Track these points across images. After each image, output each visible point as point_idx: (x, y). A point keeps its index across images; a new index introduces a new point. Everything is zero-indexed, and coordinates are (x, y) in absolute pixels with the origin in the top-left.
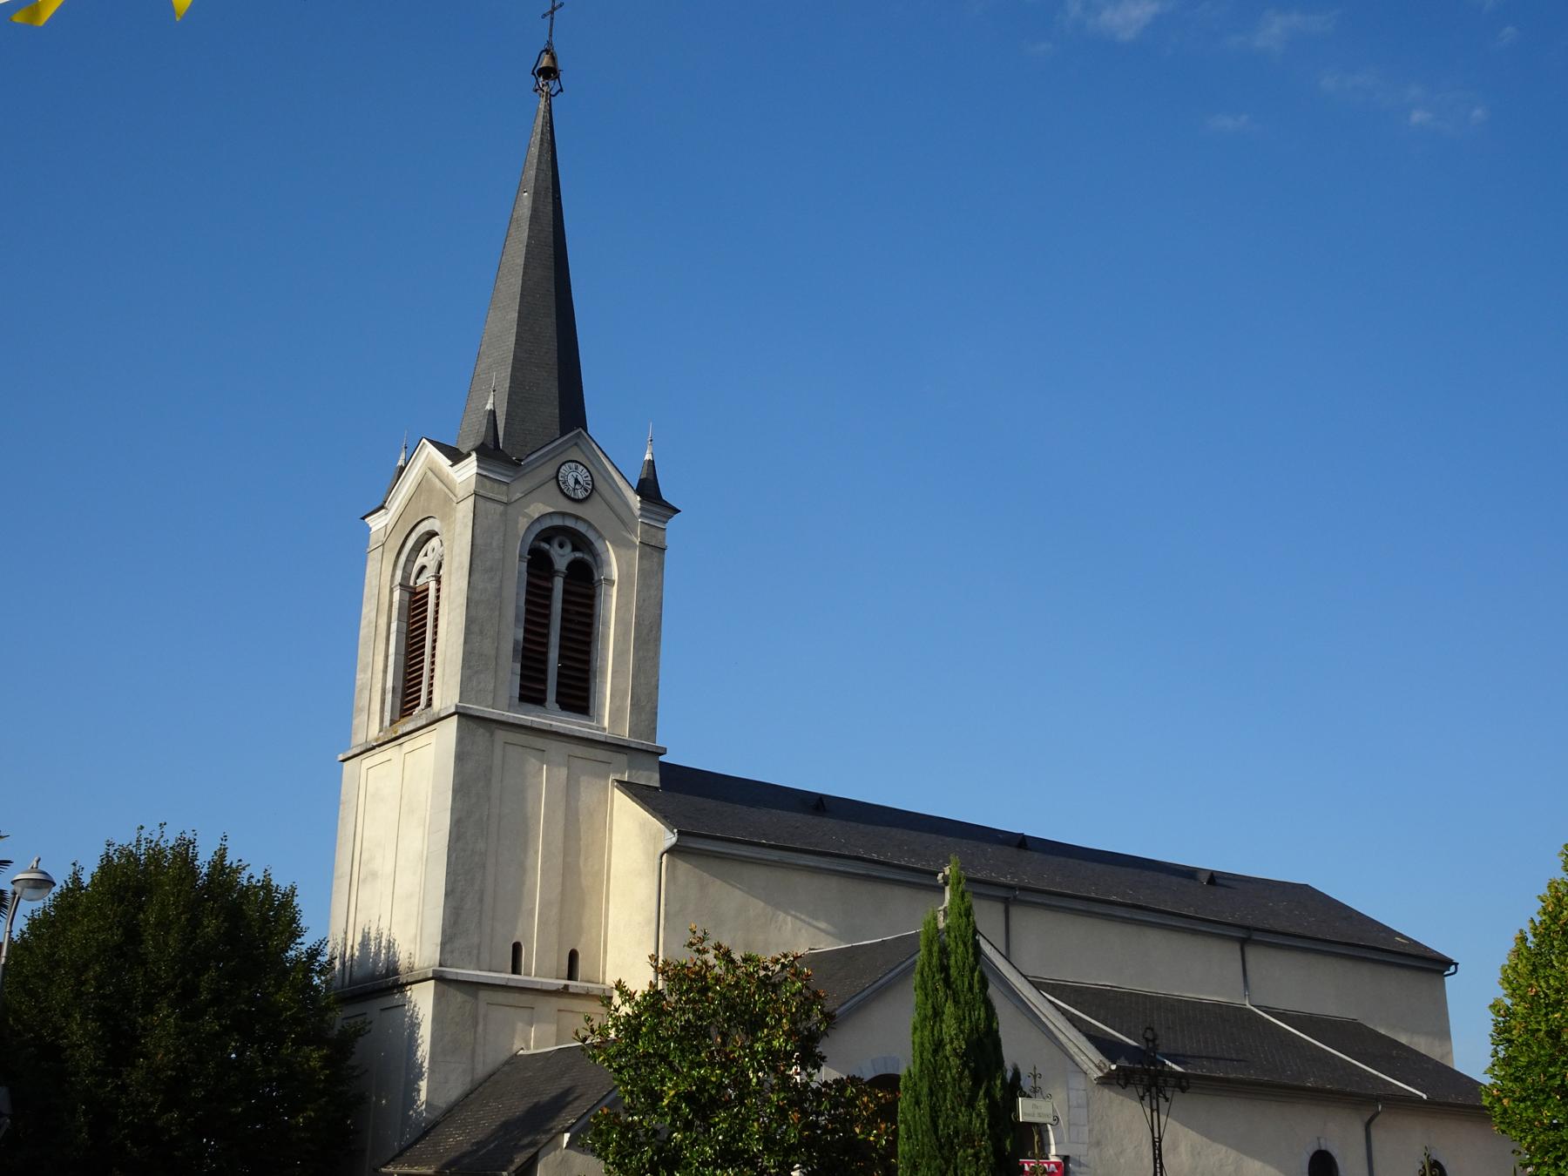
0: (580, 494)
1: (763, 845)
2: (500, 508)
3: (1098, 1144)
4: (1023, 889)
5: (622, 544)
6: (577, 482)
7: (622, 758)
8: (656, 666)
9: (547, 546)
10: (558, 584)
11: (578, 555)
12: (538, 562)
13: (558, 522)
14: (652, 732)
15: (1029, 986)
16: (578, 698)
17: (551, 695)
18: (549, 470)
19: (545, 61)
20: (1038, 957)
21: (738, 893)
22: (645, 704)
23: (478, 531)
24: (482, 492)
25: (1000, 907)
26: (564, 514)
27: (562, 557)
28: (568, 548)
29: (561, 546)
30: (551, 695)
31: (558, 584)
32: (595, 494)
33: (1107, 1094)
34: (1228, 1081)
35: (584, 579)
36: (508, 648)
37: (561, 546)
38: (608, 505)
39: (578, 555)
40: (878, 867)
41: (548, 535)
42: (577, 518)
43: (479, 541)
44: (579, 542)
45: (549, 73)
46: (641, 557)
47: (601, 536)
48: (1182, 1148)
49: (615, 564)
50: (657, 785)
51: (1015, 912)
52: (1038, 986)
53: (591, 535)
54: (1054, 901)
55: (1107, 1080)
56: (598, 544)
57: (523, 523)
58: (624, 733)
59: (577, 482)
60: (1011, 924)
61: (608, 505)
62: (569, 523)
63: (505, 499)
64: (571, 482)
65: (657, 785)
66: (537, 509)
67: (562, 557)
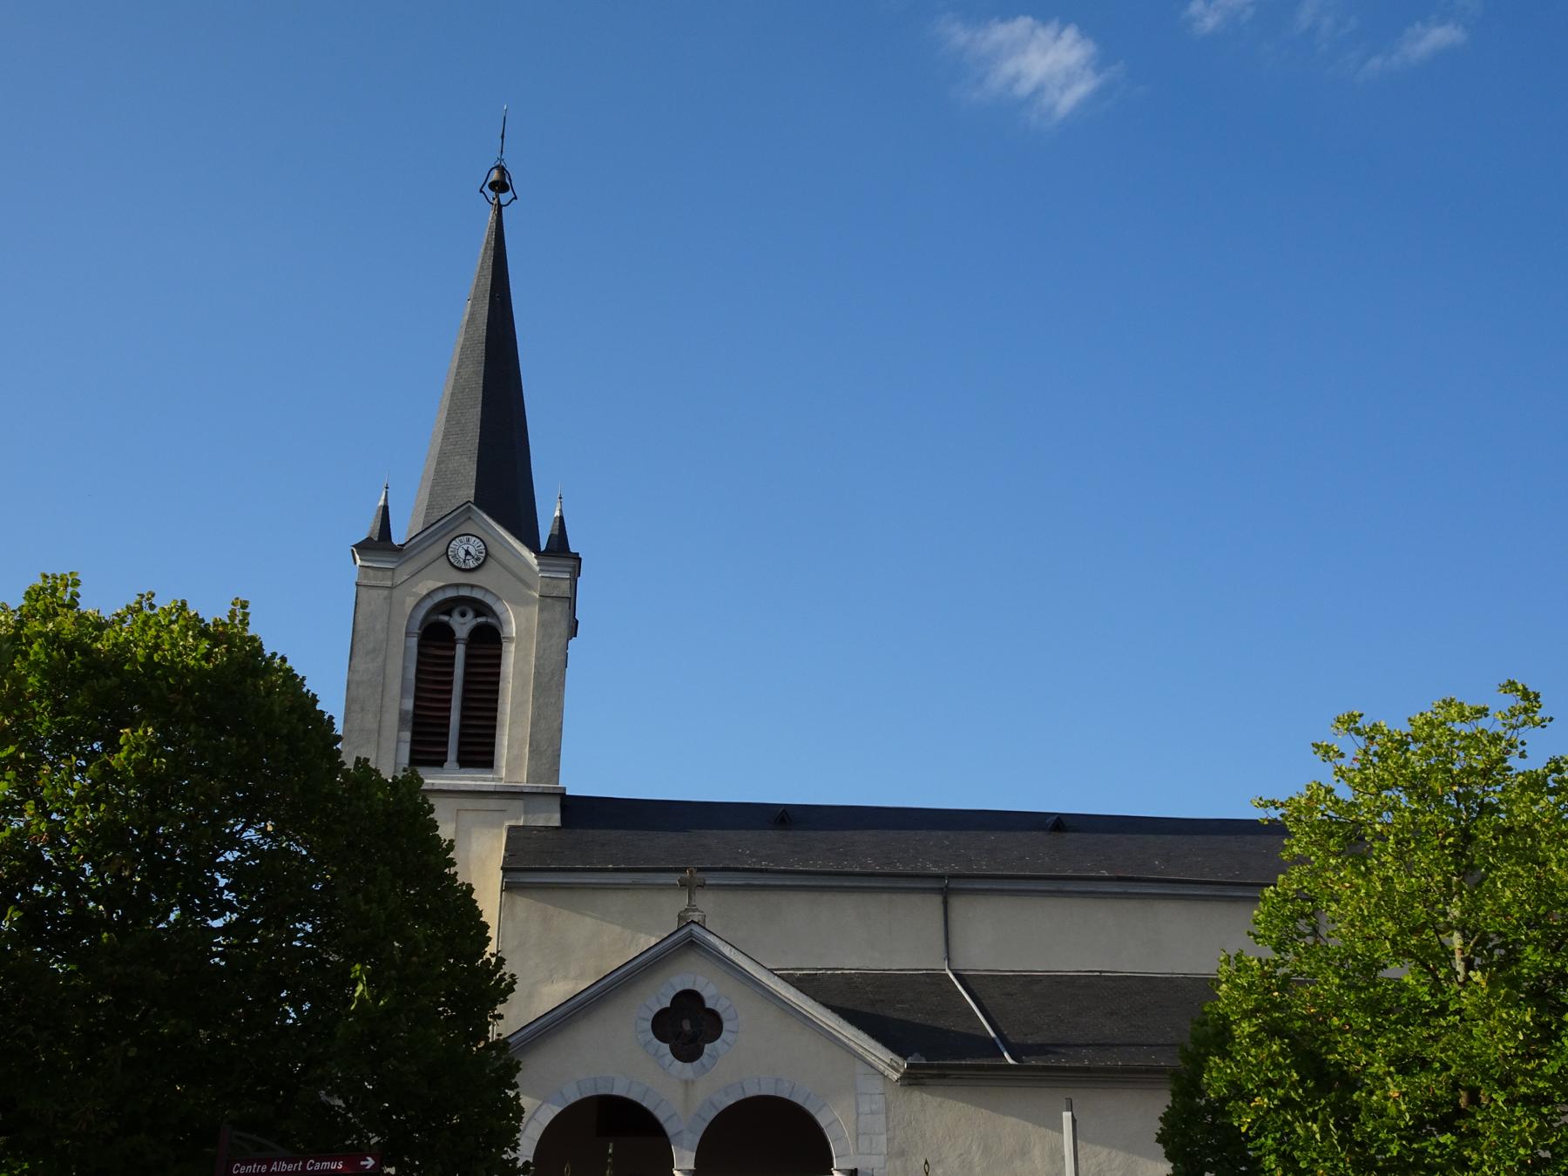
0: (472, 564)
1: (607, 870)
2: (386, 592)
3: (902, 1153)
4: (953, 877)
5: (520, 601)
6: (467, 553)
7: (518, 804)
8: (560, 711)
9: (445, 618)
10: (460, 650)
11: (481, 620)
12: (433, 636)
13: (451, 593)
14: (555, 772)
15: (780, 981)
16: (479, 753)
17: (452, 754)
18: (439, 548)
19: (495, 176)
20: (771, 944)
21: (588, 920)
22: (546, 748)
23: (360, 618)
24: (365, 582)
25: (937, 900)
26: (457, 586)
27: (463, 626)
28: (470, 615)
29: (463, 615)
30: (452, 754)
31: (460, 650)
32: (491, 563)
33: (918, 1097)
34: (1064, 1069)
35: (488, 639)
36: (392, 719)
37: (463, 615)
38: (506, 568)
39: (481, 620)
40: (717, 874)
41: (448, 606)
42: (472, 586)
43: (360, 627)
44: (481, 608)
45: (500, 186)
46: (541, 610)
47: (499, 599)
48: (1036, 1152)
49: (516, 622)
50: (558, 824)
51: (959, 905)
52: (804, 983)
53: (489, 600)
54: (1006, 885)
55: (912, 1079)
56: (497, 607)
57: (411, 602)
58: (522, 780)
59: (467, 553)
60: (953, 915)
61: (506, 568)
62: (464, 592)
63: (389, 583)
64: (462, 554)
65: (558, 824)
66: (424, 587)
67: (463, 626)
